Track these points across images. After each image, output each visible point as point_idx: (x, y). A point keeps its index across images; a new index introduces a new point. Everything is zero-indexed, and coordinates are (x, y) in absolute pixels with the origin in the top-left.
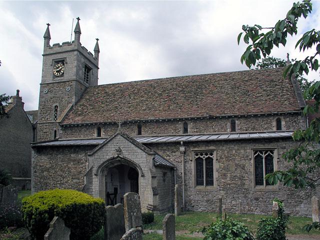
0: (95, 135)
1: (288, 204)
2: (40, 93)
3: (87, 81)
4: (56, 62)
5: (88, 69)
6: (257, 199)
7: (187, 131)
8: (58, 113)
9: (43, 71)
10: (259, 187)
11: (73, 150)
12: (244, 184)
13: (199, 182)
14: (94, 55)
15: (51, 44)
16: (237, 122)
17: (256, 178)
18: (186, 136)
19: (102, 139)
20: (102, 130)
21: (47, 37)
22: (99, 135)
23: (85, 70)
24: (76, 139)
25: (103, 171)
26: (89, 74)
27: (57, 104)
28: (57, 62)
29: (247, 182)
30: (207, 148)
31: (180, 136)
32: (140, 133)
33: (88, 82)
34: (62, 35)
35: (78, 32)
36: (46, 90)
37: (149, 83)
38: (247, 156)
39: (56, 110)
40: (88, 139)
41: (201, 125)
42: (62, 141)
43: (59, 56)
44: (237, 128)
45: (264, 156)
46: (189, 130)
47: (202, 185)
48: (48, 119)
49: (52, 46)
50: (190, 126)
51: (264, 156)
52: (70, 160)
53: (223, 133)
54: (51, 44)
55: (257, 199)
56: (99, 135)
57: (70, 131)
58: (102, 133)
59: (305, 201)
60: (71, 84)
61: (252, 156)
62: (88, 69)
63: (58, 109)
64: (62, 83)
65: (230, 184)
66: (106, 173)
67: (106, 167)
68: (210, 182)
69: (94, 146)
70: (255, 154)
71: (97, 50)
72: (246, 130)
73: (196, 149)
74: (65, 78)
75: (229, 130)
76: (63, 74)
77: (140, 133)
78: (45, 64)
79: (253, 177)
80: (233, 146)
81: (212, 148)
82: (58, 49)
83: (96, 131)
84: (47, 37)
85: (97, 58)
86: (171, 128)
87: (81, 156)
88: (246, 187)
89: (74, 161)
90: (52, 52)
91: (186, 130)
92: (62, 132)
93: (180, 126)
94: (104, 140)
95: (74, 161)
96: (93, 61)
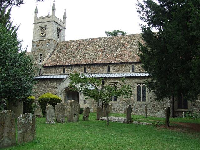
0: (62, 72)
1: (152, 112)
2: (32, 47)
3: (59, 37)
4: (41, 28)
5: (59, 30)
6: (137, 108)
7: (110, 71)
8: (42, 59)
9: (34, 33)
10: (139, 102)
11: (50, 81)
12: (131, 100)
13: (139, 99)
14: (63, 21)
15: (39, 16)
16: (135, 66)
17: (138, 97)
18: (109, 73)
19: (65, 75)
20: (66, 70)
21: (36, 12)
22: (64, 72)
23: (58, 32)
24: (52, 74)
25: (64, 93)
26: (60, 34)
27: (42, 54)
28: (42, 28)
29: (133, 99)
30: (115, 81)
31: (105, 73)
32: (85, 71)
33: (59, 38)
34: (44, 12)
35: (54, 9)
36: (35, 45)
37: (93, 40)
38: (133, 86)
39: (41, 57)
40: (58, 75)
41: (117, 67)
42: (44, 75)
43: (43, 25)
44: (135, 69)
45: (141, 86)
46: (110, 70)
47: (140, 101)
48: (36, 62)
49: (39, 18)
50: (111, 67)
51: (141, 86)
52: (48, 87)
53: (127, 72)
54: (39, 17)
55: (137, 108)
56: (64, 72)
57: (48, 70)
58: (66, 71)
59: (160, 110)
60: (50, 41)
61: (136, 86)
62: (59, 30)
63: (42, 57)
64: (44, 41)
65: (124, 100)
66: (65, 93)
67: (65, 90)
68: (144, 100)
69: (62, 79)
70: (137, 85)
71: (65, 17)
72: (140, 71)
73: (110, 82)
74: (46, 38)
75: (131, 70)
76: (45, 35)
77: (85, 71)
78: (35, 29)
79: (136, 97)
80: (127, 81)
81: (117, 81)
82: (42, 20)
83: (62, 70)
84: (36, 12)
85: (64, 23)
86: (101, 69)
87: (54, 84)
88: (132, 102)
89: (51, 87)
90: (39, 22)
91: (109, 71)
92: (44, 70)
93: (106, 68)
94: (67, 76)
95: (51, 87)
96: (62, 24)
